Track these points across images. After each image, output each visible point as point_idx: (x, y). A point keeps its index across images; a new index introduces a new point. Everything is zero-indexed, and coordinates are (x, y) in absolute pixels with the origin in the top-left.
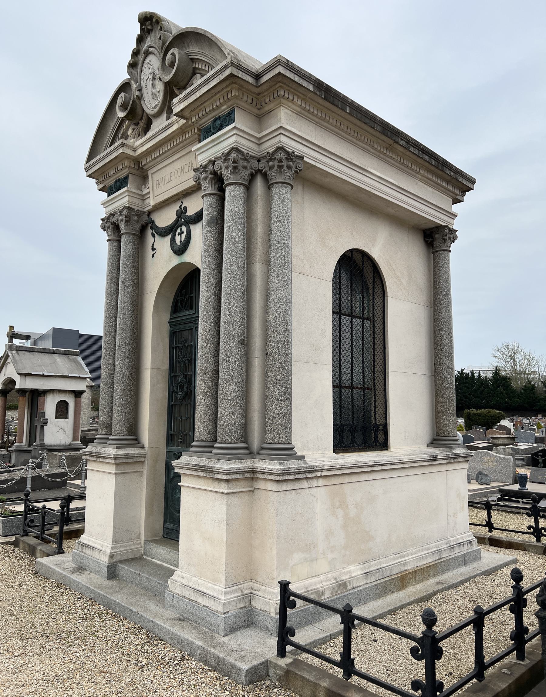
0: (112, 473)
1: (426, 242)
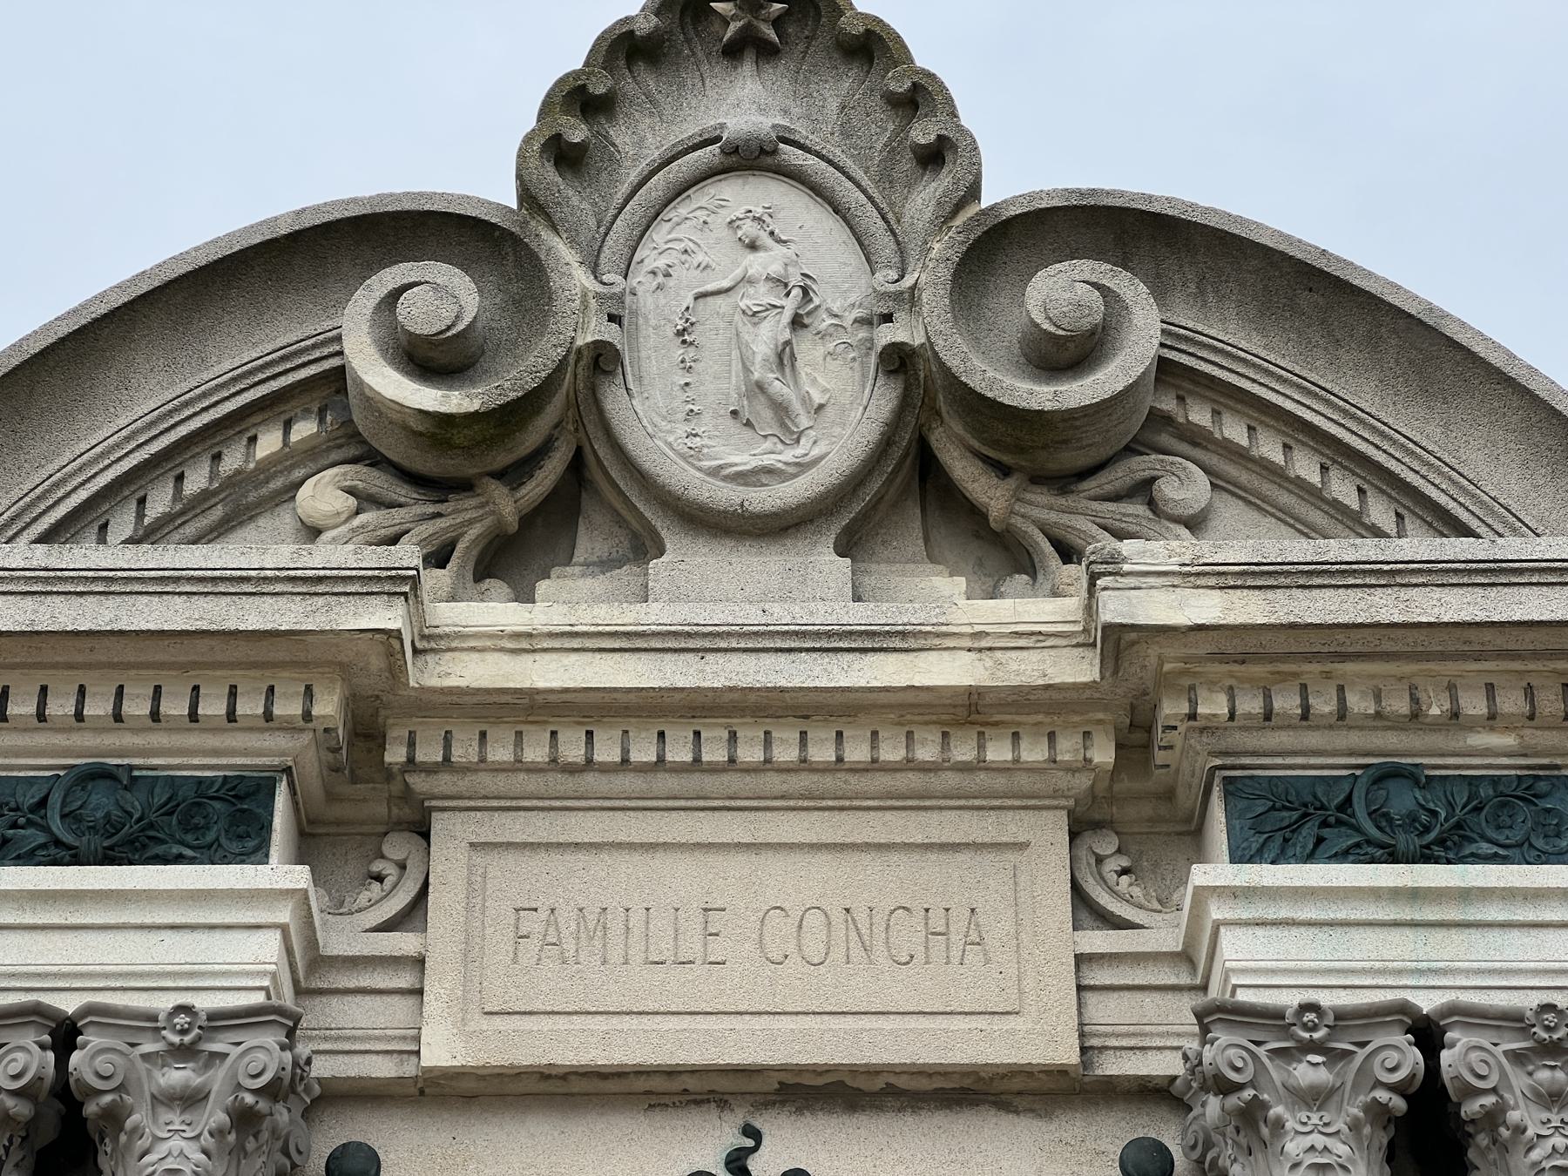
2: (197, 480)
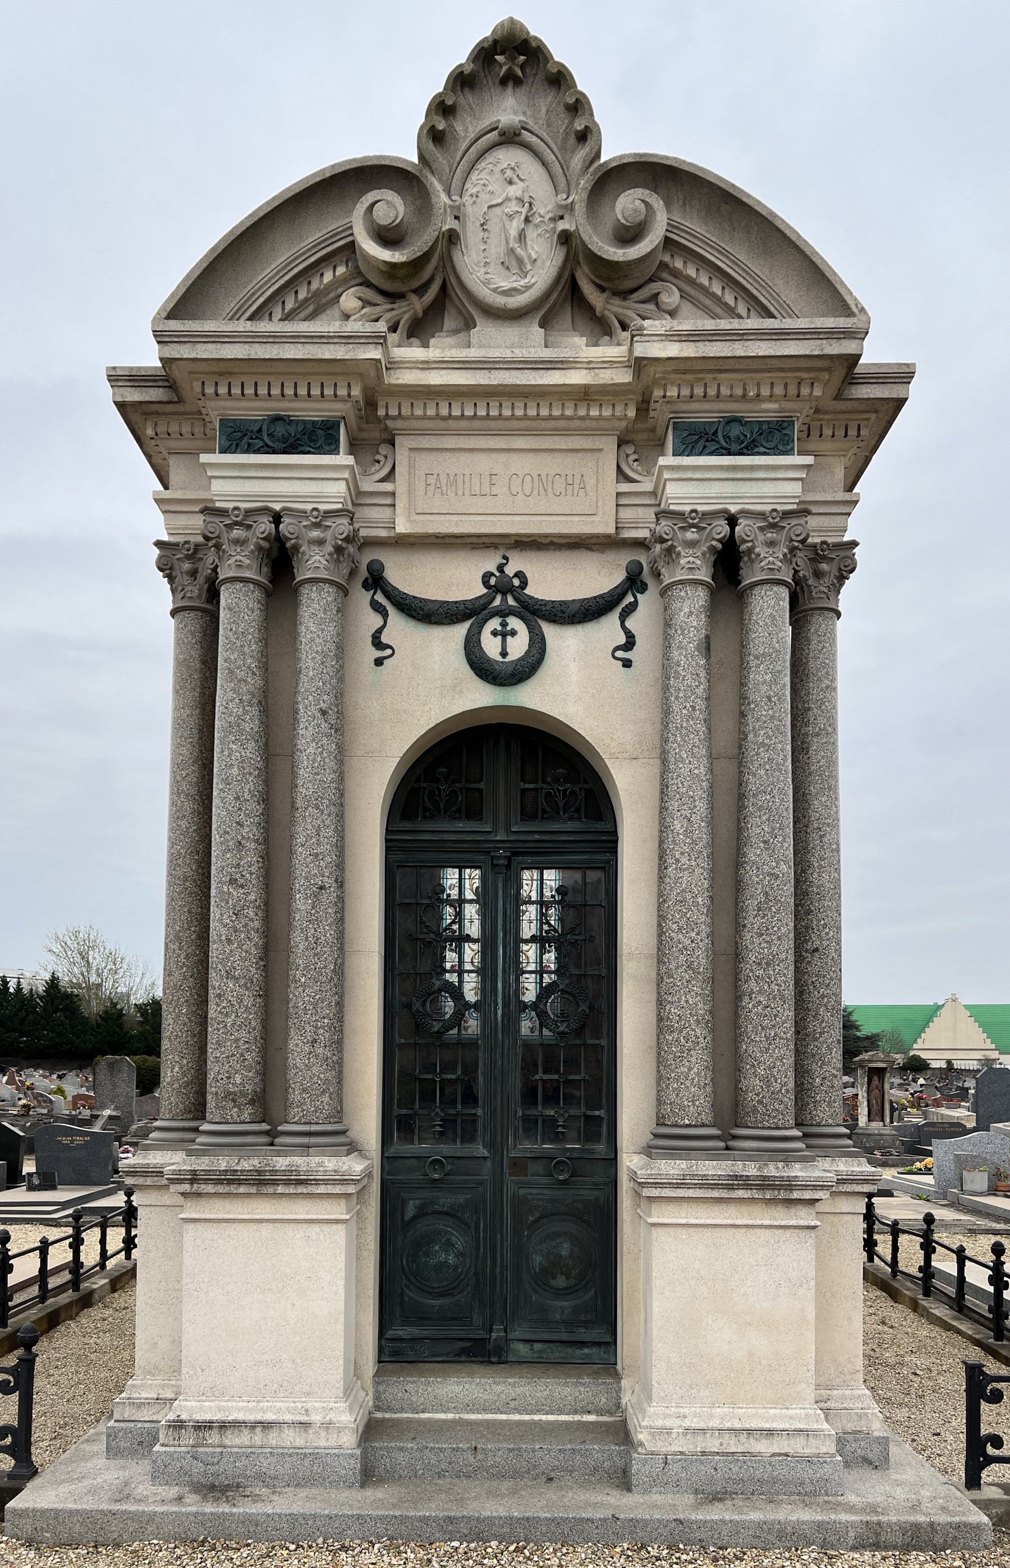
0: (337, 1221)
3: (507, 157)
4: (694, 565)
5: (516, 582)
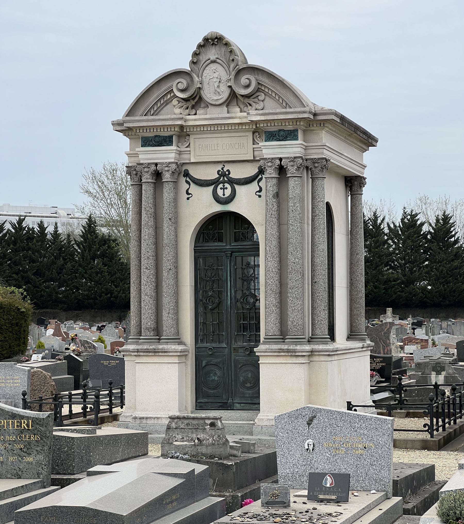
0: (176, 363)
1: (346, 186)
2: (162, 102)
3: (213, 66)
4: (271, 172)
5: (227, 173)
